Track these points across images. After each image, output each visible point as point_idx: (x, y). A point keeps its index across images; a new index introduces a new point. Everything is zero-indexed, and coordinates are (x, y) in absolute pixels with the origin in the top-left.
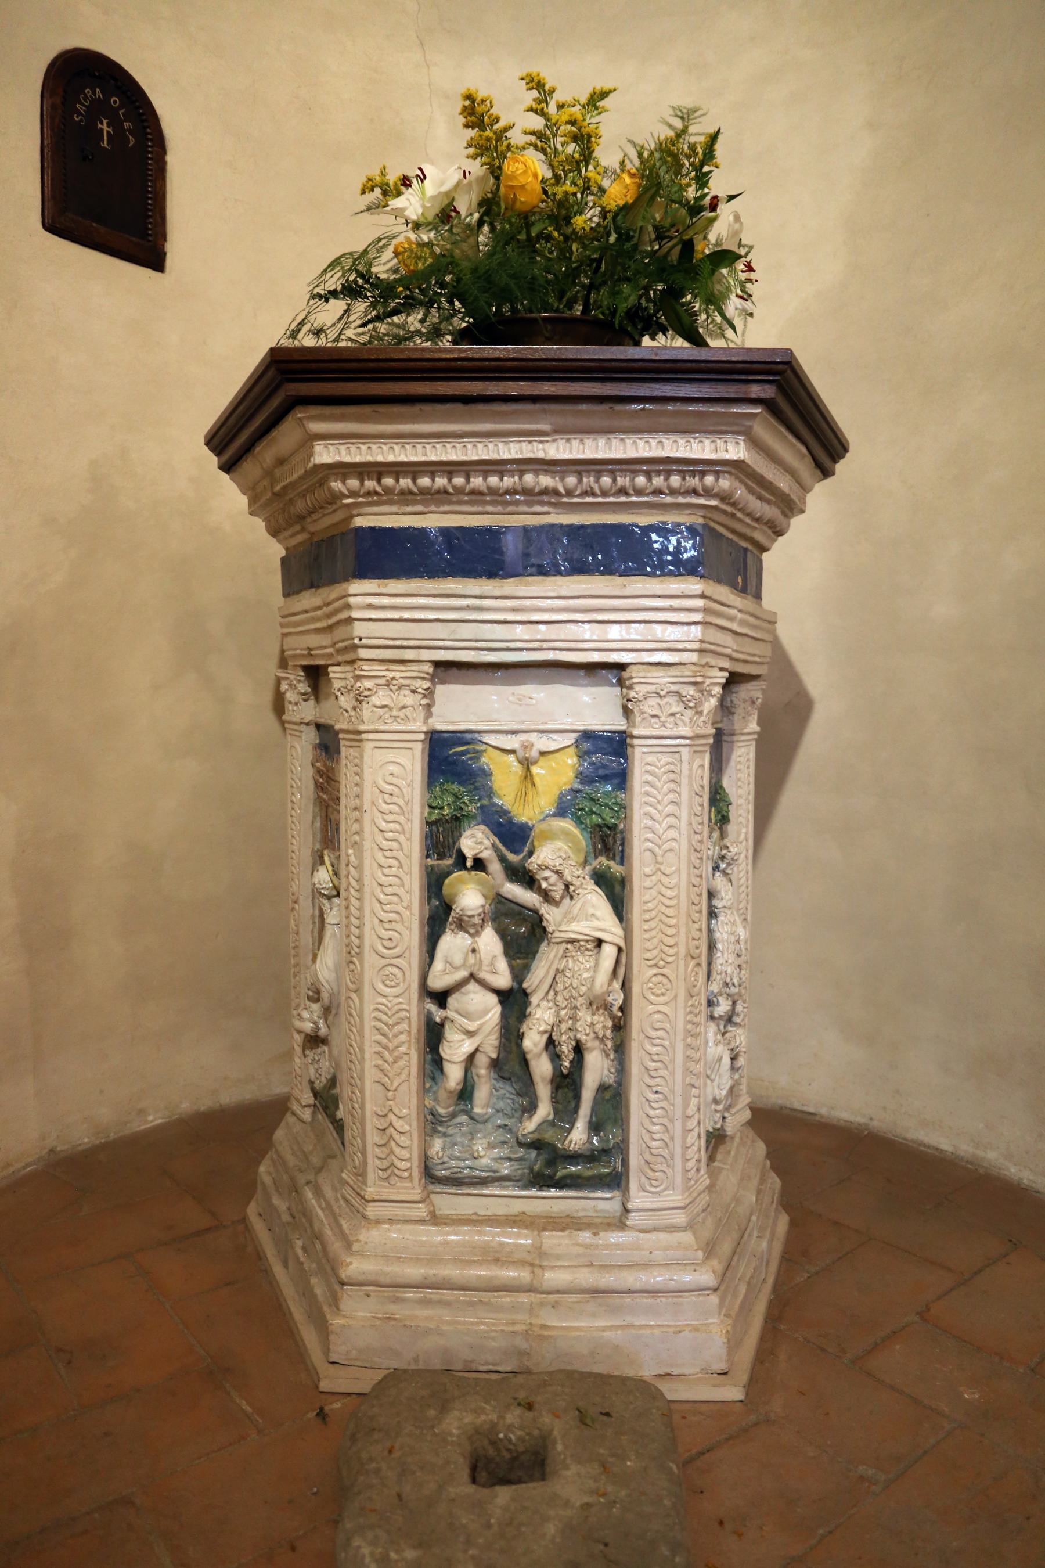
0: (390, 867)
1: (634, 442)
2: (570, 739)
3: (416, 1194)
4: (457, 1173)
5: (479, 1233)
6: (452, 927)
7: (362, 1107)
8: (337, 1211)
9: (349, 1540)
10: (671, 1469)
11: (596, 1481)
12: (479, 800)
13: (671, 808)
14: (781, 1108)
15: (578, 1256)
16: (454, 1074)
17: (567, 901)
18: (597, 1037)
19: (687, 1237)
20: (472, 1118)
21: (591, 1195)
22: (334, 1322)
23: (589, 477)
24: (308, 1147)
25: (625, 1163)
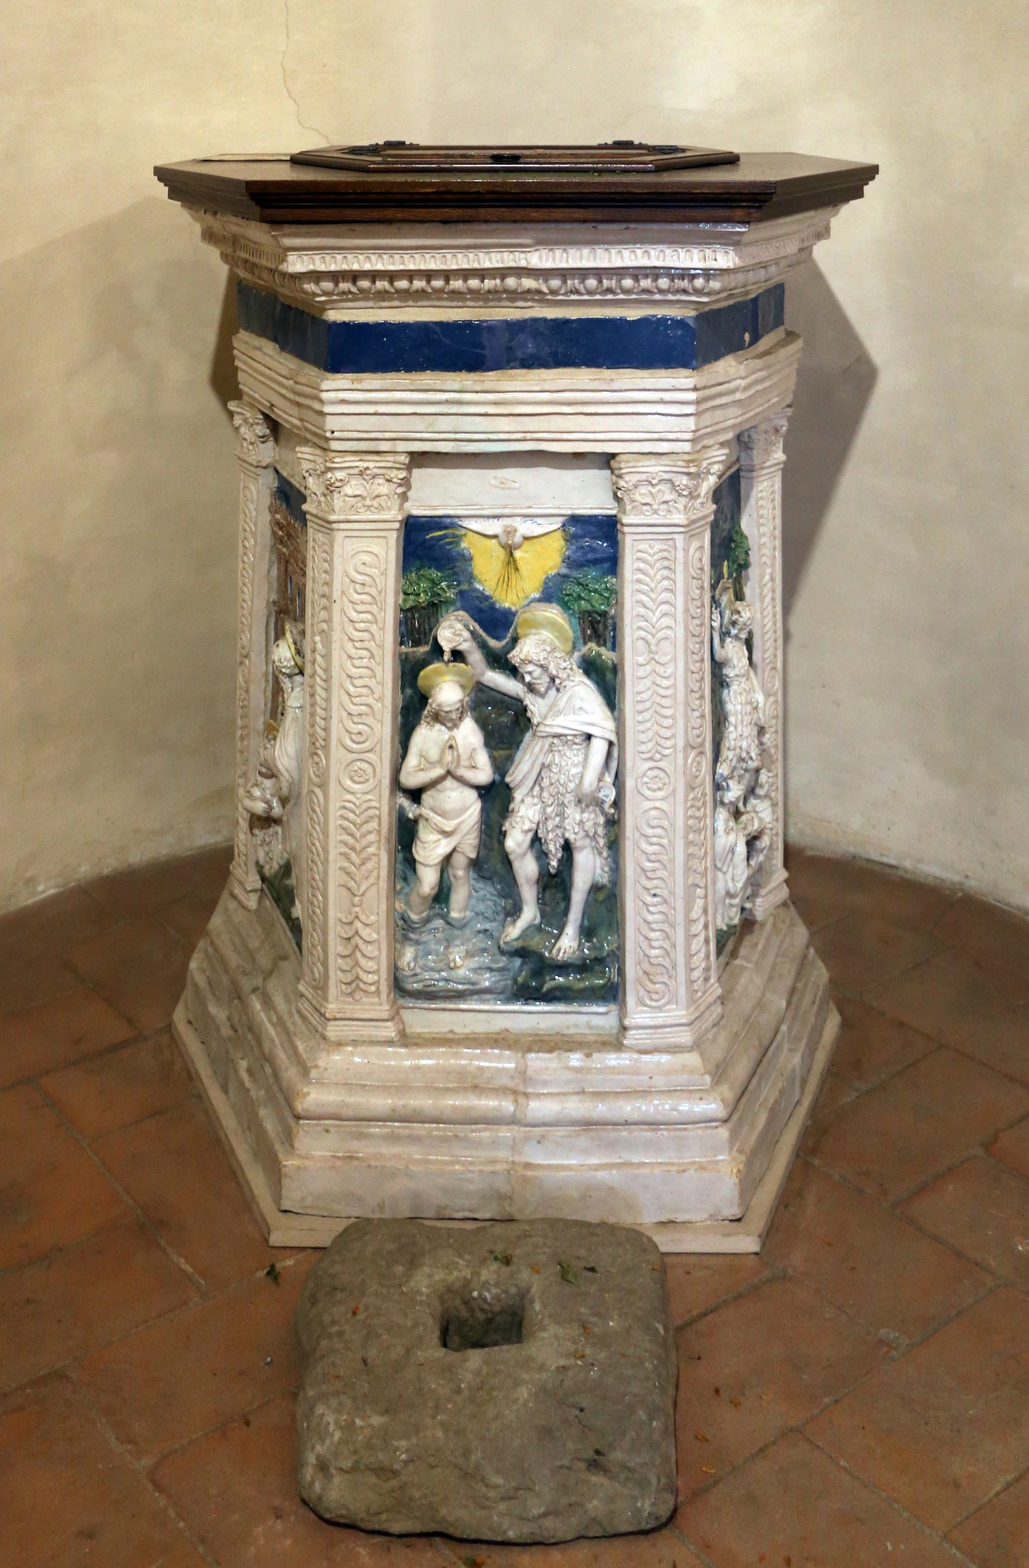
0: (361, 658)
1: (620, 252)
2: (556, 524)
3: (384, 1010)
4: (430, 986)
5: (456, 1055)
6: (428, 720)
7: (325, 913)
8: (291, 1029)
9: (312, 1408)
10: (657, 1330)
11: (575, 1343)
12: (458, 585)
13: (665, 596)
14: (854, 857)
15: (568, 1082)
16: (428, 878)
17: (553, 692)
18: (587, 835)
19: (693, 1059)
20: (448, 923)
21: (584, 1009)
22: (288, 1163)
23: (573, 279)
24: (254, 943)
25: (621, 972)
